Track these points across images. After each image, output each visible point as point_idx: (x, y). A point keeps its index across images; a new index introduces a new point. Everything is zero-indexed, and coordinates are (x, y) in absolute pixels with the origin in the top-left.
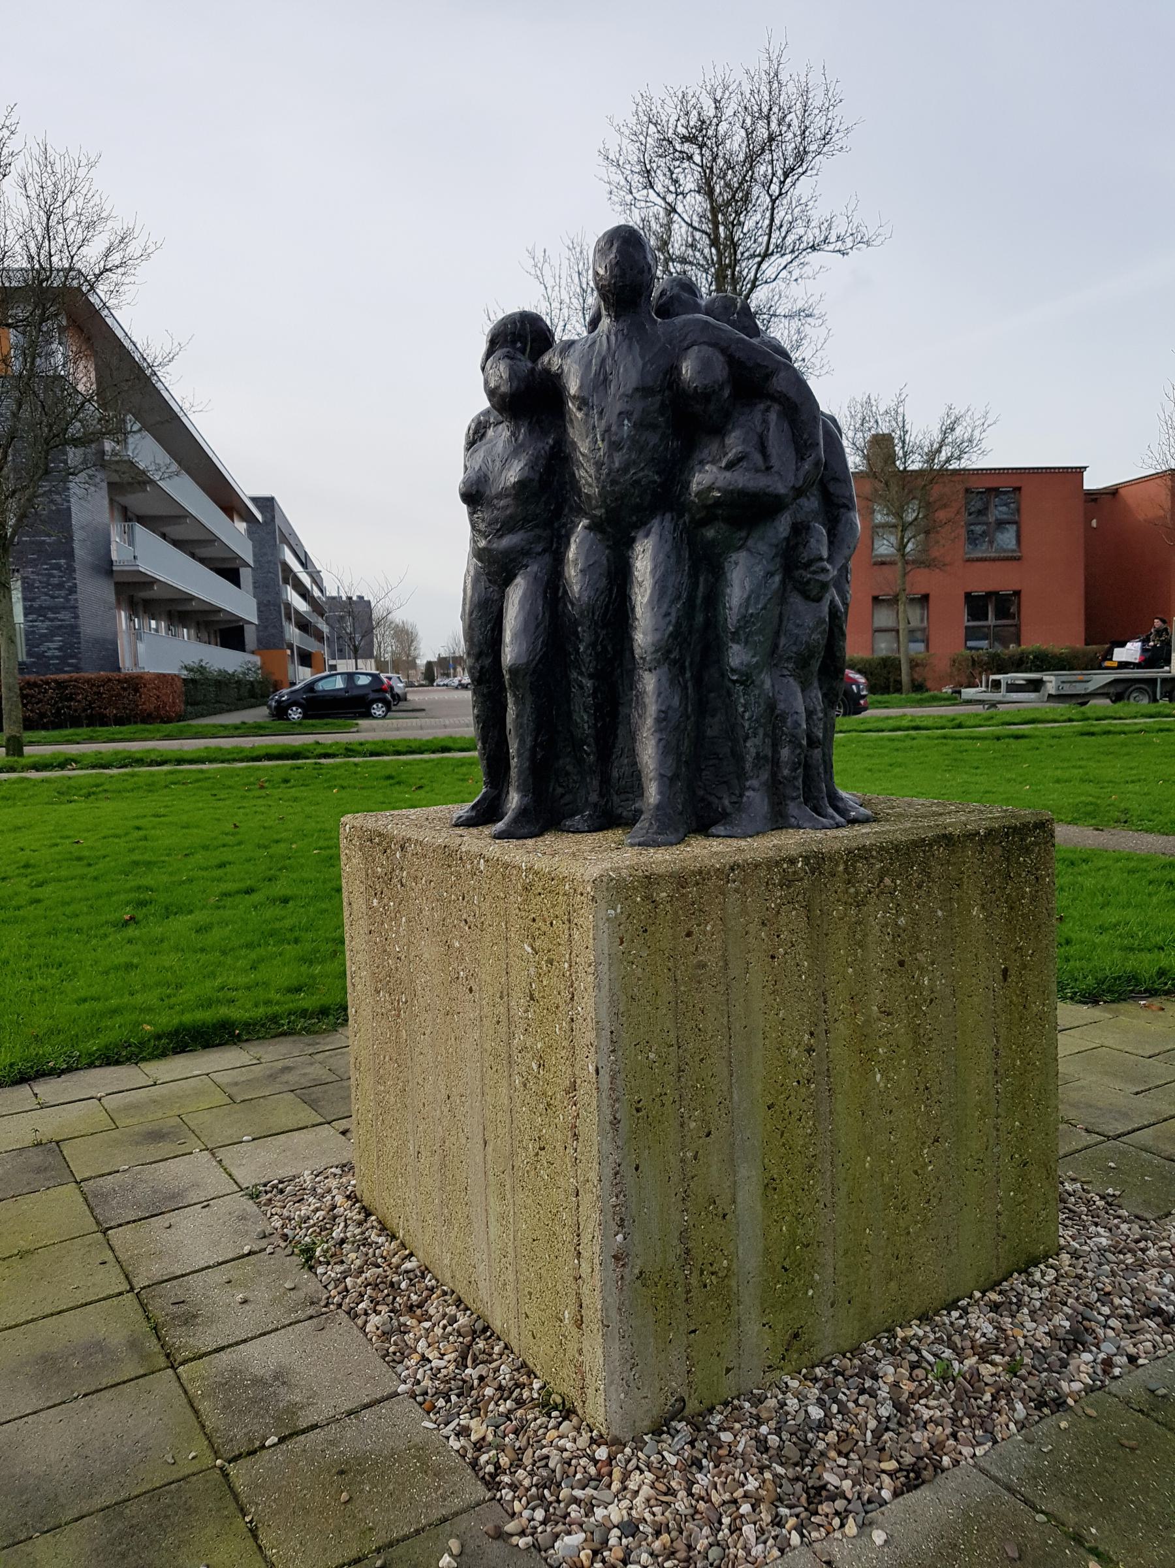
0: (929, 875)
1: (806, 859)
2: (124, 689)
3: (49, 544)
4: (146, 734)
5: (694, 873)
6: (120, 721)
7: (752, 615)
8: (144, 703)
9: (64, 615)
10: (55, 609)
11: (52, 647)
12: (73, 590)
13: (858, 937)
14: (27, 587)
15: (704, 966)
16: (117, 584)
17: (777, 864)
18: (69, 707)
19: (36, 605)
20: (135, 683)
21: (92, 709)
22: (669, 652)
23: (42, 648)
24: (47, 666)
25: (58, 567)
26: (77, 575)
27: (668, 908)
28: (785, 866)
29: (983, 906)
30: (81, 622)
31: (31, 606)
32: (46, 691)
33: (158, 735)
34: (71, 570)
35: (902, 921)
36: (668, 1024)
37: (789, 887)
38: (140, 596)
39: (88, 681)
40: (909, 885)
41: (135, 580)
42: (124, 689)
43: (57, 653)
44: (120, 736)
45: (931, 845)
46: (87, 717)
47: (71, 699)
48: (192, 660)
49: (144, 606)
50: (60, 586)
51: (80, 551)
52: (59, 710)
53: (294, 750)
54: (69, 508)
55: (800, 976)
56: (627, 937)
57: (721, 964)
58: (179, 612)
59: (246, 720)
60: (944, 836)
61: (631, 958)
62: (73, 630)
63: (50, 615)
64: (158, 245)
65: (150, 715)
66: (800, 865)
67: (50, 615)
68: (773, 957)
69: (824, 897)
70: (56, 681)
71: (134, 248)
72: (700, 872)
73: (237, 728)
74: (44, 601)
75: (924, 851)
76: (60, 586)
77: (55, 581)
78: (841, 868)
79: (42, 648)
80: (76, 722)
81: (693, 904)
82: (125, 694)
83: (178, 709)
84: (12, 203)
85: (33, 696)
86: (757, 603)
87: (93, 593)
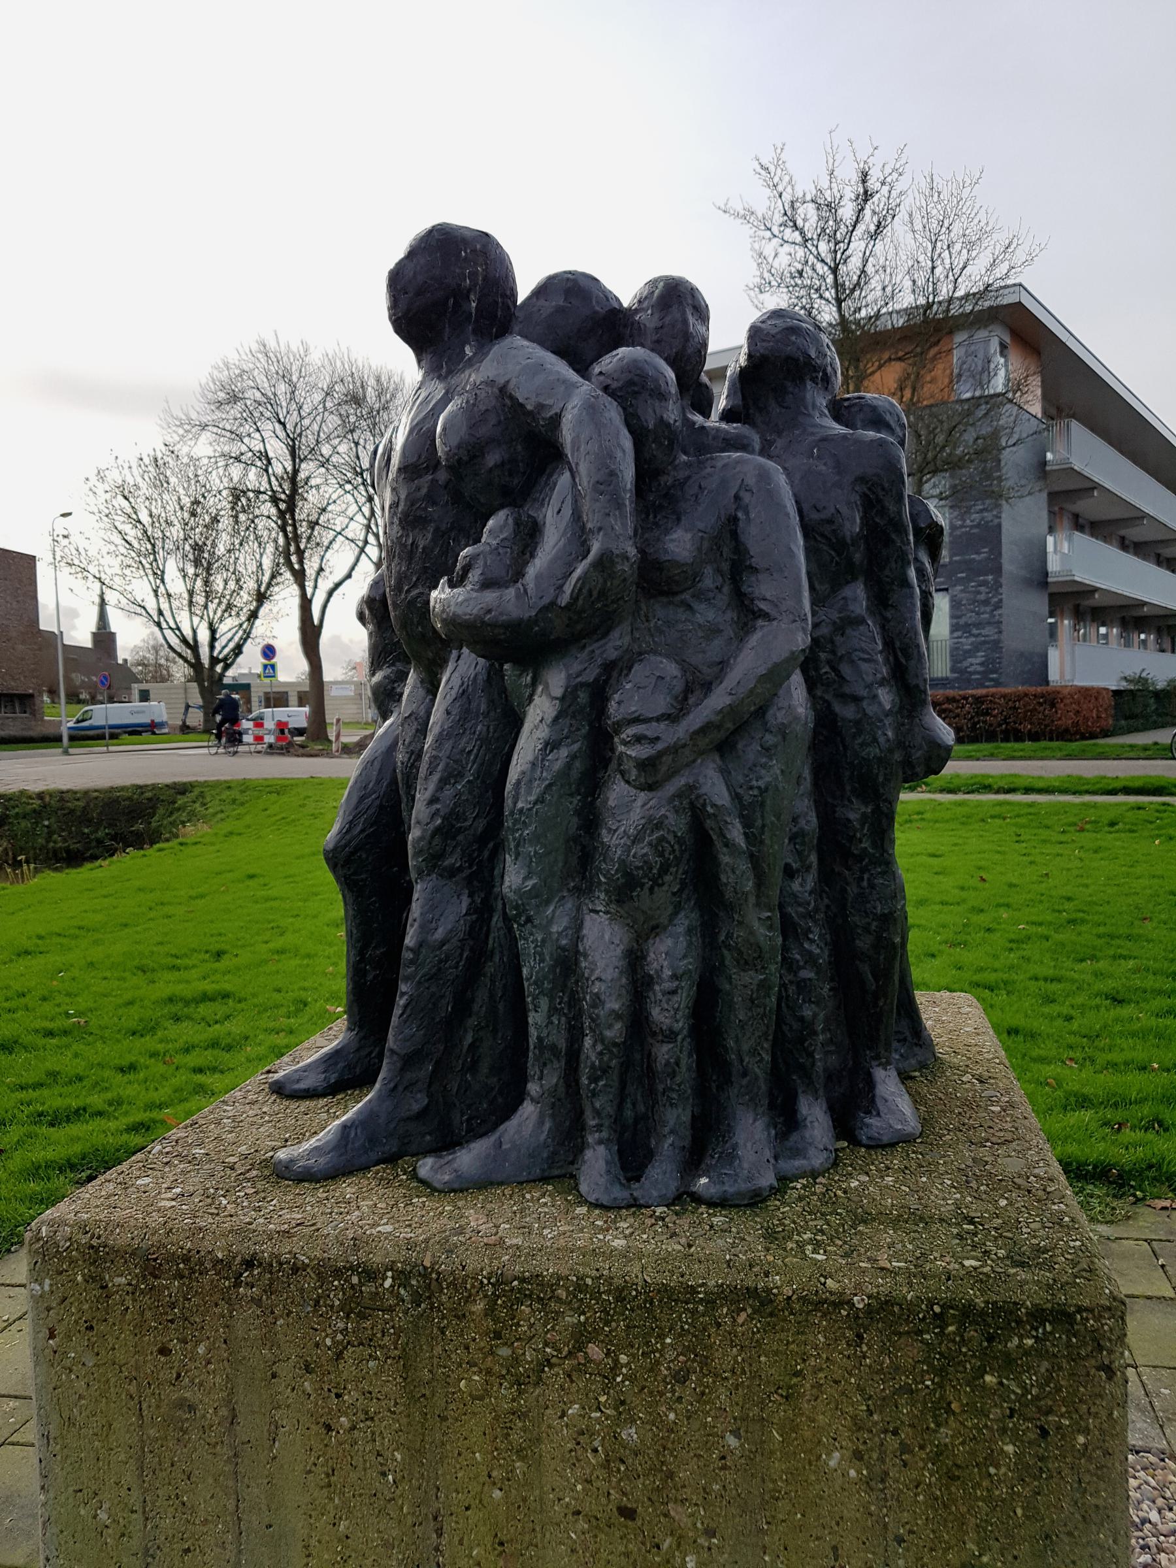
0: (705, 1362)
1: (402, 1277)
2: (1041, 704)
3: (980, 562)
4: (1048, 753)
5: (172, 1258)
6: (1035, 737)
7: (521, 811)
8: (1060, 719)
9: (989, 631)
10: (978, 625)
11: (975, 663)
12: (998, 605)
13: (516, 1437)
14: (955, 605)
15: (192, 1408)
16: (1051, 595)
17: (338, 1273)
18: (985, 722)
19: (962, 621)
20: (1052, 699)
21: (1008, 724)
22: (441, 856)
23: (965, 664)
24: (969, 681)
25: (984, 583)
26: (1004, 590)
27: (129, 1302)
28: (355, 1280)
29: (858, 1455)
30: (1004, 637)
31: (957, 624)
32: (963, 707)
33: (1059, 755)
34: (998, 585)
35: (630, 1434)
36: (129, 1478)
37: (362, 1316)
38: (1081, 605)
39: (1004, 696)
40: (654, 1368)
41: (1070, 590)
42: (1041, 704)
43: (980, 669)
44: (1021, 753)
45: (710, 1302)
46: (1002, 732)
47: (987, 714)
48: (1133, 670)
49: (1093, 615)
50: (986, 602)
51: (1008, 566)
52: (975, 724)
53: (1157, 784)
54: (999, 526)
55: (384, 1474)
56: (60, 1330)
57: (224, 1412)
58: (1136, 618)
59: (1159, 741)
60: (752, 1292)
61: (67, 1363)
62: (996, 645)
63: (975, 631)
64: (1042, 246)
65: (1067, 730)
66: (388, 1283)
67: (975, 631)
68: (329, 1428)
69: (438, 1350)
70: (973, 696)
71: (1020, 256)
72: (186, 1259)
73: (1145, 748)
74: (970, 618)
75: (694, 1312)
76: (986, 602)
77: (982, 597)
78: (479, 1307)
79: (965, 664)
80: (991, 737)
81: (173, 1306)
82: (1041, 709)
83: (1103, 723)
84: (901, 239)
85: (951, 711)
86: (529, 793)
87: (1022, 611)
